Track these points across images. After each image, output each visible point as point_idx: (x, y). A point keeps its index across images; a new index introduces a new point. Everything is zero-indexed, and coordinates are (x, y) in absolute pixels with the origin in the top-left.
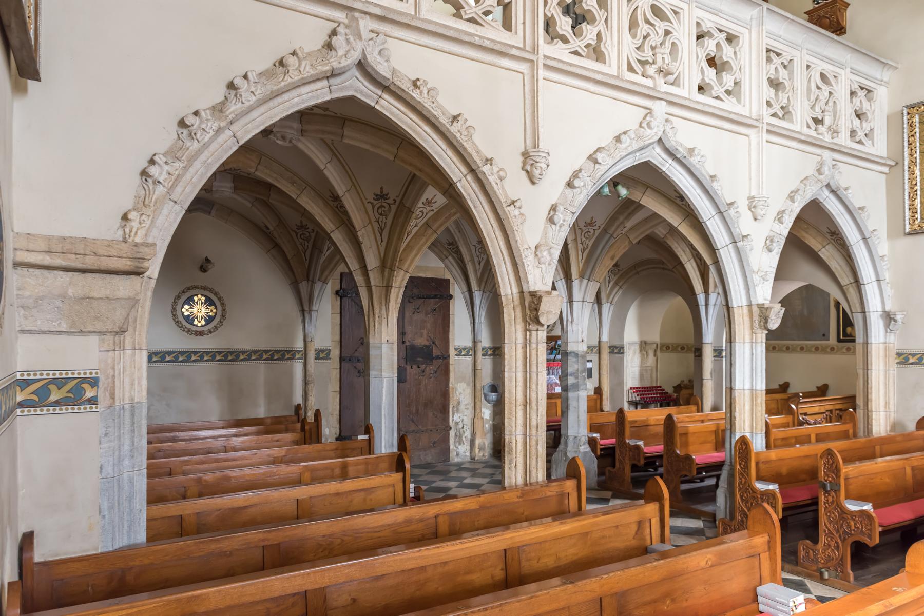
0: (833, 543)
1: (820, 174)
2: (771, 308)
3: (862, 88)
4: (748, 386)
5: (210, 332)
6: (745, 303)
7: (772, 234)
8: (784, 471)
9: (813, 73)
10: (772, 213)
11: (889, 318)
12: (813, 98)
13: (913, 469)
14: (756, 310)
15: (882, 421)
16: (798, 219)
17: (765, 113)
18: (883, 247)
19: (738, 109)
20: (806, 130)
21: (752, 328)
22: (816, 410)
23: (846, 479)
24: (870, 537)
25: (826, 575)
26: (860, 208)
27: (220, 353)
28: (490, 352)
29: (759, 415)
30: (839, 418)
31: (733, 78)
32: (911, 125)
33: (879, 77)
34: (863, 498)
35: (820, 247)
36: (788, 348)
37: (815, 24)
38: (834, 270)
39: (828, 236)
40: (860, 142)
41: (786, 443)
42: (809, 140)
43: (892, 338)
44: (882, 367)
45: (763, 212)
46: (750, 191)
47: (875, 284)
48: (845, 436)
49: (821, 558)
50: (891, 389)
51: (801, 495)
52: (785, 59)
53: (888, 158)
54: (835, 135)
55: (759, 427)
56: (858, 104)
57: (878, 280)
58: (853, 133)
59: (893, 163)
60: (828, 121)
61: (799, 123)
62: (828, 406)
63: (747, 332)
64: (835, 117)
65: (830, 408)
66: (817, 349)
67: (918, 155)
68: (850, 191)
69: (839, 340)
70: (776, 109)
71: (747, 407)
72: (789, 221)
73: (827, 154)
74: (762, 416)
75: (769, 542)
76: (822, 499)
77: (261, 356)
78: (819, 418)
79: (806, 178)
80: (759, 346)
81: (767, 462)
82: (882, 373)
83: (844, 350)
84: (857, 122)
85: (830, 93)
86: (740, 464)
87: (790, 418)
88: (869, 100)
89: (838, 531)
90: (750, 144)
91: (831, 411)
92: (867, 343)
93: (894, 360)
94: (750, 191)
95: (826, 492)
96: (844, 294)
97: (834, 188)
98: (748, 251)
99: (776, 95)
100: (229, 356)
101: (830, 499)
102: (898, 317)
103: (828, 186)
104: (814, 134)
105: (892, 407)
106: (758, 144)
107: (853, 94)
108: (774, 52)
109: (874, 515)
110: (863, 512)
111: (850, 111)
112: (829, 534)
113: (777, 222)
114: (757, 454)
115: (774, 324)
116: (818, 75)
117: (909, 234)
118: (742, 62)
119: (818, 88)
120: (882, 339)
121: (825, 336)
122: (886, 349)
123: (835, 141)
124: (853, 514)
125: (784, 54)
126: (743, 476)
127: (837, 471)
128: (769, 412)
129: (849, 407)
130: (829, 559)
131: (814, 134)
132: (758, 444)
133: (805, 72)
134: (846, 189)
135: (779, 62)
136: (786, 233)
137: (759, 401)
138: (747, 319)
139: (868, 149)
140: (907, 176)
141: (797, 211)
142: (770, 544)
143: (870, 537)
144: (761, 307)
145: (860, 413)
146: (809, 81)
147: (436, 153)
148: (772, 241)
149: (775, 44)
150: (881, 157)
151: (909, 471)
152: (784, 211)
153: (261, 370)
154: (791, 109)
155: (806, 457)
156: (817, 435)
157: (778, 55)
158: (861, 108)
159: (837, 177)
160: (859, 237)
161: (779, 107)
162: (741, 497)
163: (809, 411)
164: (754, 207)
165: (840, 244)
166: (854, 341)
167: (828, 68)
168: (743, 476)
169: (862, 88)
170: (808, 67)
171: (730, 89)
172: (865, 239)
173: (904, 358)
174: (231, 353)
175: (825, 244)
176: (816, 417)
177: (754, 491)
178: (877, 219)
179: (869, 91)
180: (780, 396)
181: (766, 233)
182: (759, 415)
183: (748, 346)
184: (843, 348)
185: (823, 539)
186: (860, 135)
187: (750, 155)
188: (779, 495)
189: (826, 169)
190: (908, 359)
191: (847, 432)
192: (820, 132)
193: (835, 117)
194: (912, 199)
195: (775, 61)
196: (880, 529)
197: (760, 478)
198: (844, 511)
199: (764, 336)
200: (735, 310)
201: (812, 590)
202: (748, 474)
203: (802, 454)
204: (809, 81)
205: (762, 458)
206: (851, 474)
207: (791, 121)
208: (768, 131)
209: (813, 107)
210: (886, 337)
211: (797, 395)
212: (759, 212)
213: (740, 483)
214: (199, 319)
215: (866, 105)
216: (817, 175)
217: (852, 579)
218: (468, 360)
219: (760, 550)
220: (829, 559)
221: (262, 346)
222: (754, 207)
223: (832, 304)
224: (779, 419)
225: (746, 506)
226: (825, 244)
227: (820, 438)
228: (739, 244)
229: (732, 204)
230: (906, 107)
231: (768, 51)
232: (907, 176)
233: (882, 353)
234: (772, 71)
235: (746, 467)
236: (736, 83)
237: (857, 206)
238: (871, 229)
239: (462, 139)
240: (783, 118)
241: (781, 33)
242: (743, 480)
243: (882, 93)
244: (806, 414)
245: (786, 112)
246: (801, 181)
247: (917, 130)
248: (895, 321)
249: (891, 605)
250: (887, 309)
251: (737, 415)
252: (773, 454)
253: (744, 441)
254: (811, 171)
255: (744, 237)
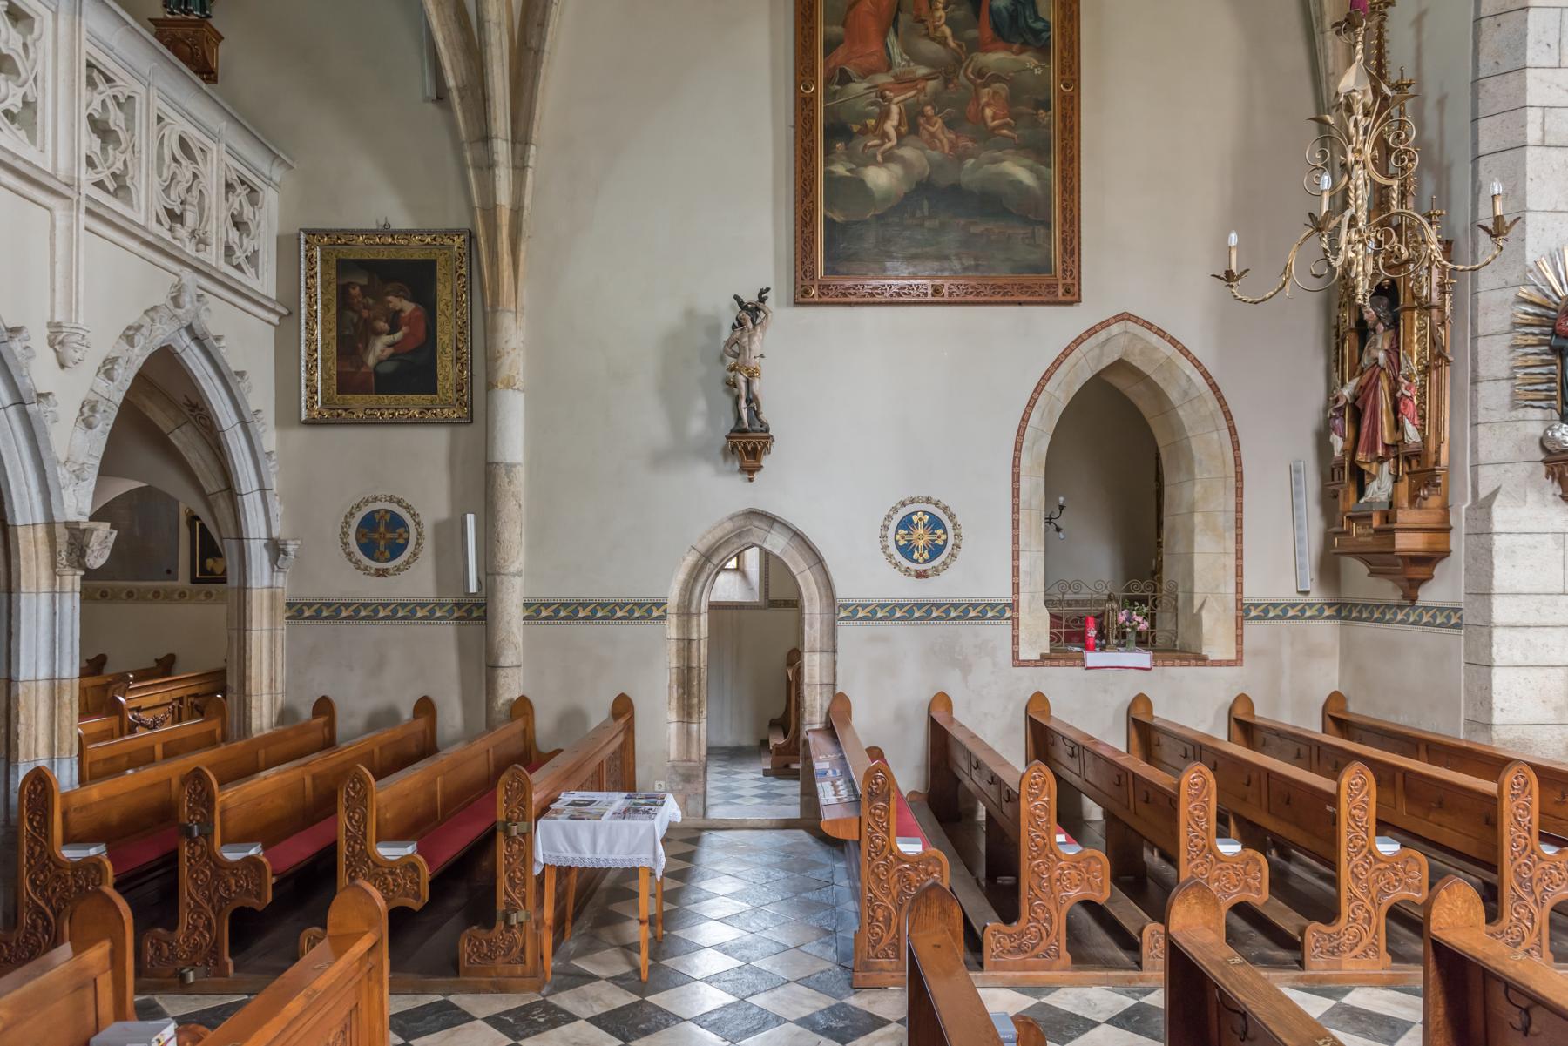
0: (201, 922)
1: (178, 306)
2: (92, 531)
3: (243, 183)
4: (44, 672)
6: (40, 518)
7: (93, 397)
8: (114, 817)
9: (166, 132)
10: (93, 360)
11: (276, 549)
12: (166, 174)
13: (314, 777)
14: (62, 535)
15: (266, 710)
16: (141, 377)
17: (83, 177)
18: (269, 439)
19: (29, 152)
20: (153, 226)
21: (54, 564)
22: (157, 700)
23: (223, 812)
24: (258, 896)
25: (191, 977)
26: (237, 373)
29: (66, 723)
30: (198, 710)
31: (21, 91)
32: (310, 260)
33: (267, 173)
34: (246, 838)
35: (172, 427)
36: (104, 595)
37: (168, 47)
38: (194, 467)
39: (186, 410)
40: (238, 267)
41: (112, 769)
42: (161, 244)
43: (281, 580)
44: (266, 626)
45: (78, 355)
46: (53, 311)
47: (257, 495)
48: (209, 741)
49: (183, 952)
50: (279, 658)
51: (146, 854)
52: (123, 90)
53: (278, 301)
54: (201, 246)
55: (66, 746)
56: (236, 205)
57: (262, 490)
58: (229, 251)
59: (285, 312)
60: (191, 218)
61: (144, 207)
62: (177, 691)
63: (44, 574)
64: (201, 216)
65: (178, 694)
66: (156, 594)
67: (318, 307)
68: (223, 343)
69: (194, 580)
70: (104, 175)
71: (43, 712)
72: (125, 376)
73: (188, 275)
74: (72, 725)
75: (112, 952)
76: (185, 852)
78: (160, 713)
79: (154, 308)
80: (67, 597)
81: (85, 807)
82: (266, 634)
83: (202, 597)
84: (234, 234)
85: (195, 176)
86: (31, 821)
87: (115, 720)
88: (253, 203)
89: (210, 900)
90: (53, 226)
91: (181, 700)
92: (245, 588)
93: (282, 613)
94: (53, 311)
95: (192, 840)
96: (210, 508)
97: (198, 333)
98: (48, 424)
99: (104, 150)
101: (198, 850)
102: (290, 548)
103: (189, 328)
104: (167, 236)
105: (279, 685)
106: (70, 228)
107: (229, 186)
108: (100, 71)
109: (265, 860)
110: (251, 861)
111: (224, 214)
112: (197, 910)
113: (102, 376)
114: (65, 796)
115: (98, 557)
116: (175, 138)
117: (306, 423)
118: (39, 68)
119: (175, 160)
120: (266, 582)
121: (171, 573)
122: (272, 597)
123: (201, 255)
124: (233, 866)
125: (118, 82)
126: (37, 842)
127: (209, 801)
128: (85, 713)
129: (218, 689)
130: (196, 948)
131: (167, 236)
132: (66, 776)
133: (155, 128)
134: (218, 339)
135: (110, 92)
136: (118, 398)
137: (66, 698)
138: (43, 549)
139: (248, 279)
140: (303, 335)
141: (139, 362)
142: (116, 958)
143: (258, 896)
144: (72, 527)
145: (233, 699)
146: (161, 143)
147: (20, 494)
148: (93, 409)
149: (103, 58)
150: (269, 299)
151: (308, 781)
152: (115, 360)
154: (128, 183)
155: (153, 786)
156: (165, 745)
157: (108, 80)
158: (241, 213)
159: (204, 316)
160: (236, 420)
161: (108, 172)
162: (33, 882)
163: (145, 703)
164: (61, 343)
165: (205, 426)
166: (224, 581)
167: (192, 133)
168: (37, 842)
169: (243, 183)
170: (160, 119)
171: (15, 111)
172: (244, 423)
173: (297, 611)
175: (180, 421)
176: (154, 712)
177: (59, 864)
178: (261, 395)
179: (253, 190)
180: (100, 684)
181: (82, 394)
182: (66, 723)
183: (44, 599)
184: (198, 593)
185: (186, 918)
186: (239, 256)
187: (53, 245)
188: (108, 863)
189: (185, 299)
191: (211, 733)
192: (178, 235)
193: (201, 216)
194: (311, 371)
195: (101, 88)
196: (274, 880)
197: (69, 840)
198: (220, 865)
199: (77, 579)
200: (20, 531)
201: (167, 1010)
202: (48, 836)
203: (146, 782)
204: (161, 143)
205: (75, 802)
206: (231, 804)
207: (129, 202)
208: (89, 212)
209: (166, 190)
210: (272, 578)
211: (122, 678)
212: (71, 354)
213: (32, 855)
215: (248, 211)
216: (171, 306)
217: (231, 970)
219: (95, 972)
220: (196, 948)
222: (61, 343)
223: (183, 518)
224: (97, 723)
225: (43, 896)
226: (180, 421)
227: (171, 751)
228: (31, 409)
229: (16, 330)
230: (307, 231)
231: (90, 65)
232: (303, 335)
233: (266, 603)
234: (97, 104)
235: (46, 822)
236: (26, 103)
237: (234, 369)
238: (253, 409)
240: (115, 194)
241: (113, 43)
242: (38, 849)
243: (270, 197)
244: (138, 709)
245: (121, 187)
246: (146, 312)
247: (318, 269)
248: (286, 554)
249: (315, 992)
250: (275, 535)
251: (22, 729)
252: (95, 792)
253: (40, 779)
254: (162, 298)
255: (40, 395)
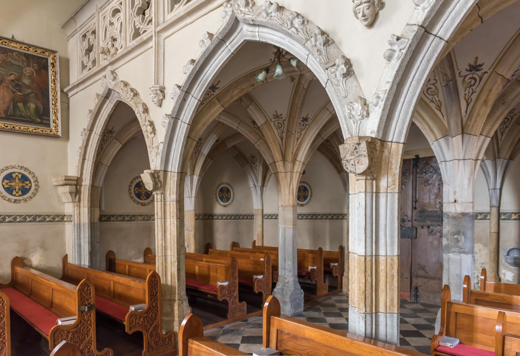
5: (306, 204)
27: (310, 215)
28: (201, 217)
77: (327, 217)
100: (313, 217)
153: (327, 224)
174: (314, 215)
190: (46, 218)
214: (17, 190)
218: (503, 209)
221: (327, 211)
239: (406, 43)
